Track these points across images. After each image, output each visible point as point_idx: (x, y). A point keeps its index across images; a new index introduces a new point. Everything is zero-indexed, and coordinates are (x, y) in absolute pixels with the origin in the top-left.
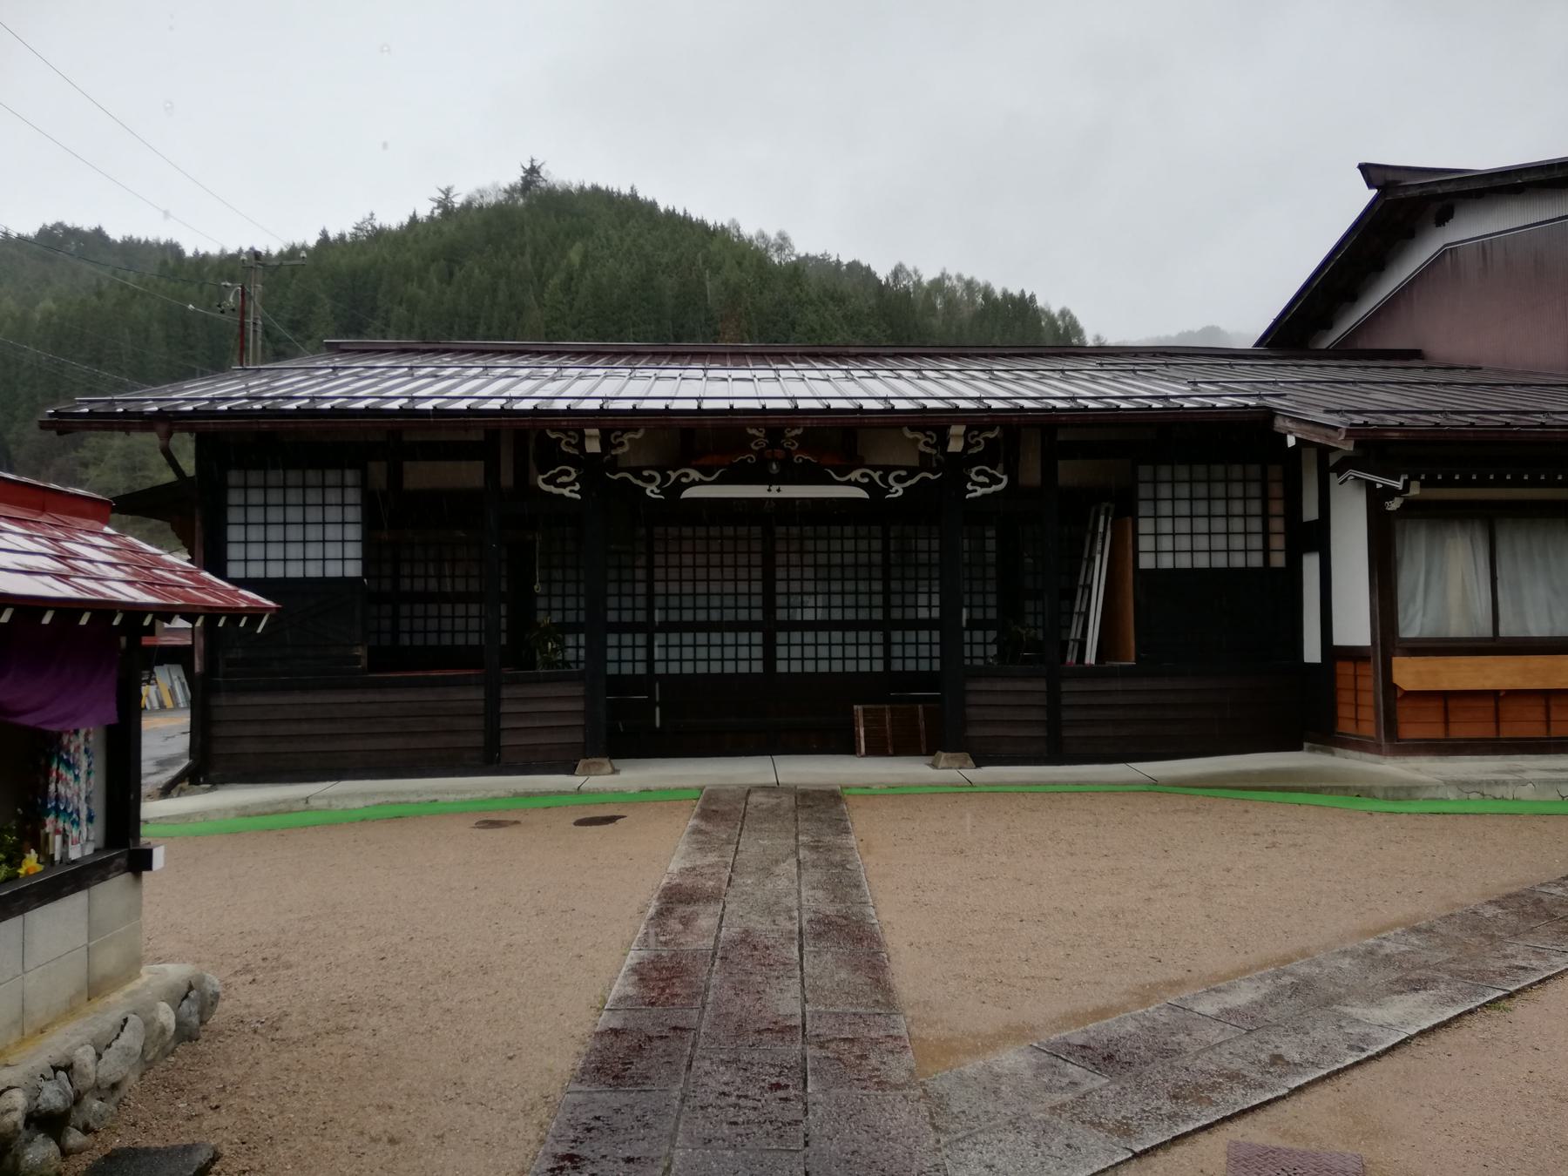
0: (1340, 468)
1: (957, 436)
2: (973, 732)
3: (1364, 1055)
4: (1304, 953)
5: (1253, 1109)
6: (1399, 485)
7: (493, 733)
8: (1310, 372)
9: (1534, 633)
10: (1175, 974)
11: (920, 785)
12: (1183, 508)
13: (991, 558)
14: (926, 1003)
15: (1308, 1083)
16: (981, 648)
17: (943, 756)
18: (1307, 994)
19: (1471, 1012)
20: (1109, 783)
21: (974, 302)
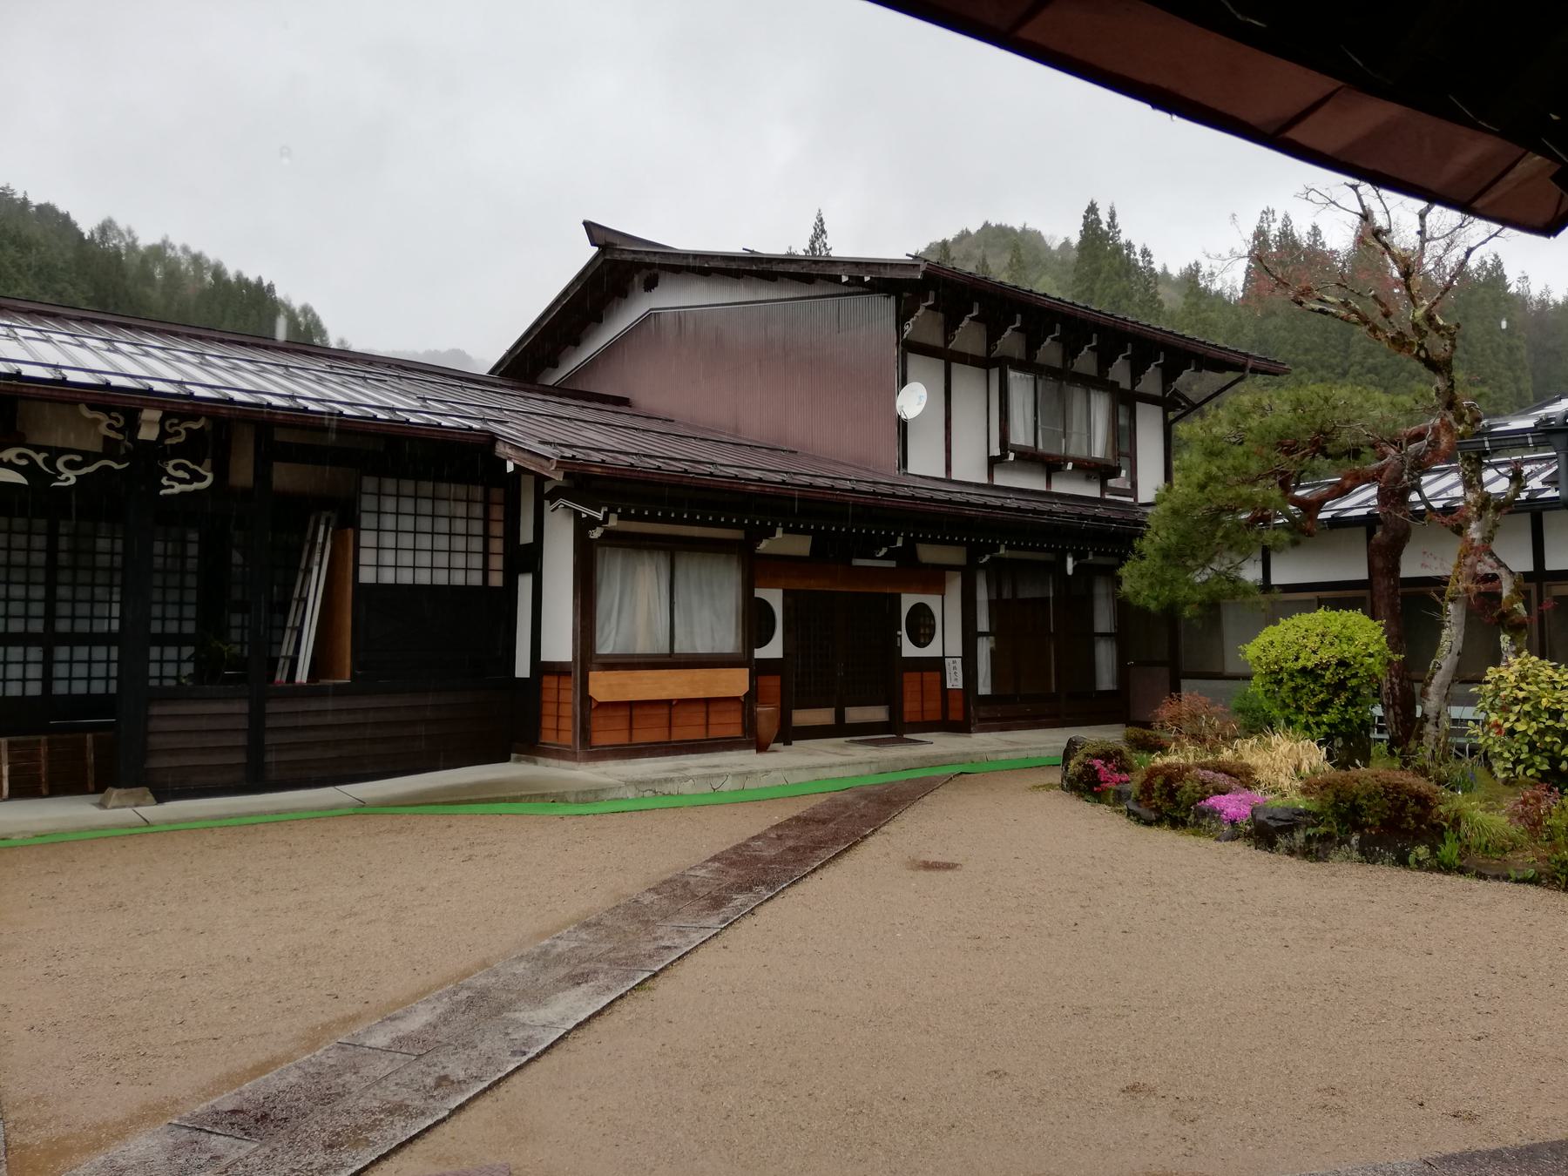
0: (555, 495)
1: (151, 422)
2: (154, 763)
3: (524, 1059)
4: (484, 964)
5: (411, 1140)
6: (600, 516)
7: (255, 749)
8: (536, 404)
9: (639, 651)
10: (351, 1009)
11: (79, 830)
12: (407, 523)
13: (192, 564)
14: (38, 1099)
15: (470, 1100)
16: (169, 665)
17: (114, 793)
18: (482, 1005)
19: (621, 997)
20: (313, 810)
21: (202, 279)
